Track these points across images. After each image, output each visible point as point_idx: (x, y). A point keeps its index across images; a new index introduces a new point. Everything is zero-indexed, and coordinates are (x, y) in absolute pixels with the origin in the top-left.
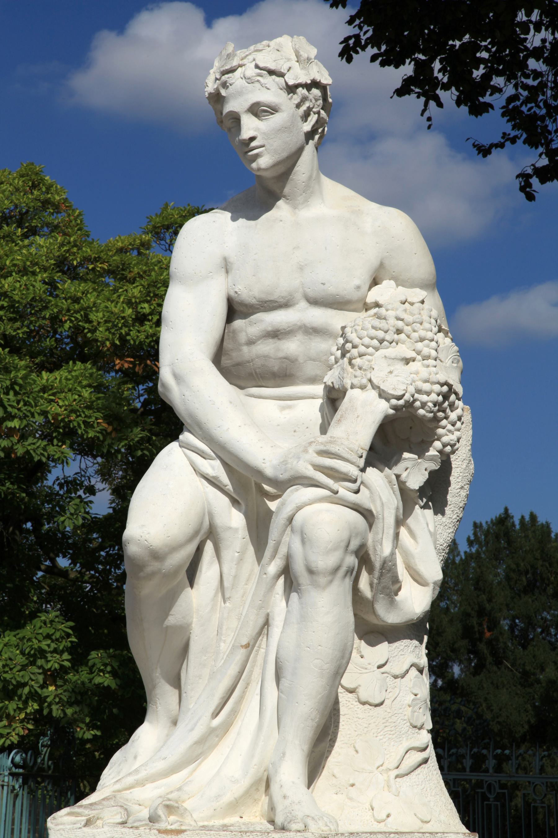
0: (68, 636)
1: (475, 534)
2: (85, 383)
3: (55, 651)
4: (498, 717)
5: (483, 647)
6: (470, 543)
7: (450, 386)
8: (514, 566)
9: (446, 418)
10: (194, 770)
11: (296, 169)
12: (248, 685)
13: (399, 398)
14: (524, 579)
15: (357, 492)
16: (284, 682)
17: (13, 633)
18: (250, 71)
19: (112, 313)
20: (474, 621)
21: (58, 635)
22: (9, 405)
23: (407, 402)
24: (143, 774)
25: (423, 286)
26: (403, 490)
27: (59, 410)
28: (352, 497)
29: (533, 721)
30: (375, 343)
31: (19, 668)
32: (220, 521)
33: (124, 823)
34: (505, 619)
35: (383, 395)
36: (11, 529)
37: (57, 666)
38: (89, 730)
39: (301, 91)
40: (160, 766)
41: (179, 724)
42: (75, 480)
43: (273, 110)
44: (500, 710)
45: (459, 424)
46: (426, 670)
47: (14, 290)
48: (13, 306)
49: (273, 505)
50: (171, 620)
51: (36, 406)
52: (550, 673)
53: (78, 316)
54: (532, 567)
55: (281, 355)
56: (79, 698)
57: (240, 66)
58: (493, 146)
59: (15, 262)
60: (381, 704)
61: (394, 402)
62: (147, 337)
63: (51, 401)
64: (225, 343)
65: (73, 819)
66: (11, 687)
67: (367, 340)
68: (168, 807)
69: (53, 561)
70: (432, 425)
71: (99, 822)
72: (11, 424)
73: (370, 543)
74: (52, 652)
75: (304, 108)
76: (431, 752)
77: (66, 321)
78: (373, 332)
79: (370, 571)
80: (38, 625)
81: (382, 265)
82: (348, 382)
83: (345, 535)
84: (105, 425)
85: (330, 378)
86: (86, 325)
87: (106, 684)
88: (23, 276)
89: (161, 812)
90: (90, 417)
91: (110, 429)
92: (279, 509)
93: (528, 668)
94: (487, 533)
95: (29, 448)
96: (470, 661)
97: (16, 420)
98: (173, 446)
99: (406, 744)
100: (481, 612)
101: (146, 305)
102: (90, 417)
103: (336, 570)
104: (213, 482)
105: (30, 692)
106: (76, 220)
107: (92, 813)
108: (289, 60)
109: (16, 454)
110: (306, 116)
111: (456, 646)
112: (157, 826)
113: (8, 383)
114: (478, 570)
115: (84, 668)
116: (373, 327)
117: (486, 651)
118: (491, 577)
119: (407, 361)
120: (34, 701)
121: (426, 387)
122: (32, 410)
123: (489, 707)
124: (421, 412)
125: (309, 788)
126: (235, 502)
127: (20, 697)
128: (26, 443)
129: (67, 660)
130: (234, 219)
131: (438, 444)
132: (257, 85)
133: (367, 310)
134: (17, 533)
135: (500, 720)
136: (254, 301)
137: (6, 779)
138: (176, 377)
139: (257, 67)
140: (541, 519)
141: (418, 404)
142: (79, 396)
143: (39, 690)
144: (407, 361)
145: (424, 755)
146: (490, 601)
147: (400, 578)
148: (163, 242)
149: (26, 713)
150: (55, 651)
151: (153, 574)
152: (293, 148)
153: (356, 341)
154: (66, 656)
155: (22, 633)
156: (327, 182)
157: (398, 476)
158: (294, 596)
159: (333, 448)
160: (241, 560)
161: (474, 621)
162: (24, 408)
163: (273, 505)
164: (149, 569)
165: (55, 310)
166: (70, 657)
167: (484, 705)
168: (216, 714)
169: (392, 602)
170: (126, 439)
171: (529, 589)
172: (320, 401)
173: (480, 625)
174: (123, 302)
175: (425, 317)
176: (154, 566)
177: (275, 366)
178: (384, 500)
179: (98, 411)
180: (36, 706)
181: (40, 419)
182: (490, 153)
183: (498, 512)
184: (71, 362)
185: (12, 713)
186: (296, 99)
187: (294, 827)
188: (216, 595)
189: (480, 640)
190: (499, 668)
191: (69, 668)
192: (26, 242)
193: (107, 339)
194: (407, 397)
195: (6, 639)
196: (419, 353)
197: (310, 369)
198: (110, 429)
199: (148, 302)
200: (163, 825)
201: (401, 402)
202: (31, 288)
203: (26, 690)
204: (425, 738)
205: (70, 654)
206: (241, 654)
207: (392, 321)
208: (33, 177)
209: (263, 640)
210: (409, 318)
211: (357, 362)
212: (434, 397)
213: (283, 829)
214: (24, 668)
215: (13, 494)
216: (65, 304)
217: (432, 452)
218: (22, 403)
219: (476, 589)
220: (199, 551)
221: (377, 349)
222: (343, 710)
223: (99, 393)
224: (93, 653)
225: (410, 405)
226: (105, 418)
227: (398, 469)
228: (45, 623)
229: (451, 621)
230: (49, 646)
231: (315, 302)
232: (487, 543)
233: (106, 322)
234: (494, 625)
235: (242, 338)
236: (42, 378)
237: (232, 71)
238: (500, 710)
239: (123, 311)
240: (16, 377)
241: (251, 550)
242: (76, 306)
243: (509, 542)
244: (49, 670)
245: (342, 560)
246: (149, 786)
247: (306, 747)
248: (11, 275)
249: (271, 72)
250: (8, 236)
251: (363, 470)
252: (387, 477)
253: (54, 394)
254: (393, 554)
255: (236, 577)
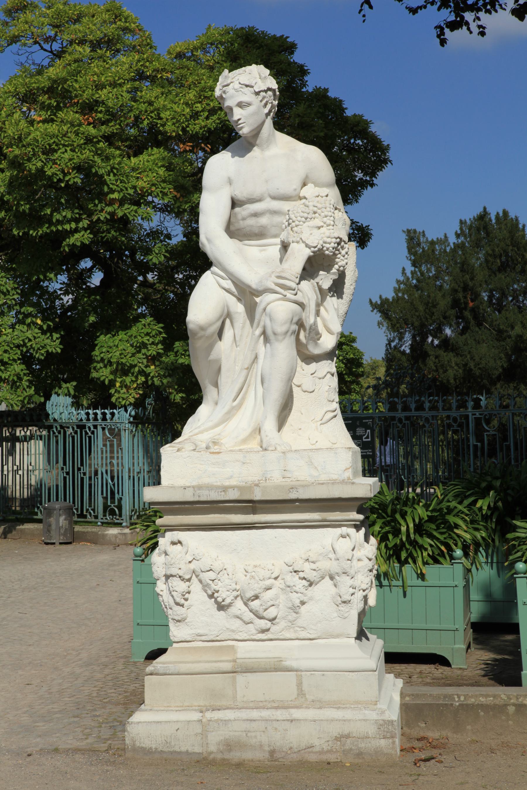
0: (160, 333)
1: (461, 229)
2: (160, 164)
3: (153, 343)
4: (479, 364)
5: (467, 314)
6: (458, 236)
7: (341, 239)
8: (490, 252)
9: (340, 253)
10: (226, 426)
11: (262, 131)
12: (249, 386)
13: (315, 247)
14: (498, 261)
15: (296, 295)
16: (265, 385)
17: (124, 332)
18: (237, 86)
19: (175, 112)
20: (461, 295)
21: (154, 333)
22: (111, 183)
23: (319, 249)
24: (202, 428)
25: (328, 186)
26: (320, 289)
27: (144, 185)
28: (293, 297)
29: (505, 365)
30: (303, 219)
31: (130, 355)
32: (232, 310)
33: (194, 450)
34: (485, 292)
35: (307, 246)
36: (116, 260)
37: (155, 353)
38: (177, 394)
39: (262, 94)
40: (210, 424)
41: (219, 405)
42: (157, 230)
43: (249, 104)
44: (481, 359)
45: (346, 256)
46: (336, 374)
47: (109, 99)
48: (109, 111)
49: (258, 300)
50: (213, 356)
51: (129, 183)
52: (518, 330)
53: (153, 115)
54: (505, 251)
55: (259, 225)
56: (171, 372)
57: (232, 82)
58: (420, 8)
59: (107, 79)
60: (313, 391)
61: (313, 249)
62: (201, 129)
63: (138, 178)
64: (231, 219)
65: (171, 449)
66: (126, 368)
67: (299, 218)
68: (214, 442)
69: (145, 277)
70: (333, 257)
71: (183, 450)
72: (112, 196)
73: (304, 317)
74: (150, 344)
75: (264, 102)
76: (339, 411)
77: (145, 119)
78: (302, 214)
79: (305, 330)
80: (140, 327)
81: (307, 177)
82: (291, 240)
83: (290, 316)
84: (175, 193)
85: (283, 236)
86: (159, 121)
87: (186, 363)
88: (114, 88)
89: (210, 445)
90: (165, 188)
91: (178, 195)
92: (261, 301)
93: (501, 327)
94: (470, 228)
95: (126, 212)
96: (458, 324)
97: (116, 193)
98: (208, 274)
99: (325, 409)
100: (465, 288)
101: (199, 105)
102: (165, 188)
103: (287, 332)
104: (228, 291)
105: (139, 371)
106: (146, 40)
107: (180, 446)
108: (255, 78)
109: (117, 216)
110: (265, 105)
111: (447, 314)
112: (209, 450)
113: (109, 168)
114: (463, 257)
115: (171, 353)
116: (302, 212)
117: (469, 317)
118: (474, 261)
119: (319, 228)
120: (142, 375)
121: (329, 240)
122: (126, 186)
123: (472, 358)
124: (327, 252)
125: (279, 432)
126: (239, 300)
127: (133, 374)
128: (124, 208)
129: (161, 349)
130: (233, 157)
131: (336, 266)
132: (240, 92)
133: (300, 200)
134: (120, 262)
135: (480, 366)
136: (244, 199)
137: (127, 426)
138: (208, 240)
139: (240, 83)
140: (512, 215)
141: (325, 249)
142: (157, 174)
143: (144, 369)
144: (319, 228)
145: (335, 413)
146: (472, 279)
147: (320, 332)
148: (208, 54)
149: (137, 384)
150: (153, 343)
151: (201, 337)
152: (260, 122)
153: (294, 219)
154: (160, 346)
155: (130, 332)
156: (278, 134)
157: (317, 283)
158: (268, 345)
159: (283, 275)
160: (243, 327)
161: (461, 295)
162: (120, 185)
163: (258, 300)
164: (199, 335)
165: (137, 112)
166: (162, 347)
167: (468, 356)
168: (235, 400)
169: (316, 344)
170: (190, 202)
171: (503, 268)
172: (279, 246)
173: (465, 297)
174: (183, 104)
175: (328, 205)
176: (201, 333)
177: (256, 231)
178: (310, 296)
179: (170, 184)
180: (143, 379)
181: (131, 191)
182: (417, 12)
183: (478, 211)
184: (150, 149)
185: (129, 384)
186: (260, 98)
187: (270, 449)
188: (232, 344)
189: (465, 308)
190: (480, 329)
191: (163, 354)
192: (114, 61)
193: (174, 131)
194: (319, 246)
195: (120, 337)
196: (325, 223)
197: (273, 231)
198: (178, 195)
199: (200, 102)
200: (212, 450)
201: (316, 249)
202: (120, 97)
203: (137, 369)
204: (336, 405)
205: (162, 345)
206: (245, 372)
207: (311, 208)
208: (115, 11)
209: (255, 365)
210: (319, 206)
211: (295, 229)
212: (333, 245)
213: (266, 450)
214: (133, 355)
215: (116, 238)
216: (143, 107)
217: (334, 270)
218: (119, 182)
219: (462, 271)
220: (223, 323)
221: (304, 222)
222: (295, 395)
223: (170, 171)
224: (176, 343)
225: (321, 250)
226: (175, 188)
227: (317, 280)
228: (145, 325)
229: (444, 296)
230: (148, 340)
231: (274, 198)
232: (470, 235)
233: (172, 119)
234: (476, 296)
235: (240, 217)
236: (131, 162)
237: (228, 85)
238: (481, 359)
239: (183, 111)
240: (114, 164)
241: (248, 322)
242: (151, 108)
243: (488, 234)
244: (150, 355)
245: (289, 328)
246: (205, 433)
247: (276, 414)
248: (106, 88)
249: (247, 86)
250: (101, 57)
251: (299, 284)
252: (312, 284)
253: (139, 173)
254: (315, 323)
255: (241, 336)
